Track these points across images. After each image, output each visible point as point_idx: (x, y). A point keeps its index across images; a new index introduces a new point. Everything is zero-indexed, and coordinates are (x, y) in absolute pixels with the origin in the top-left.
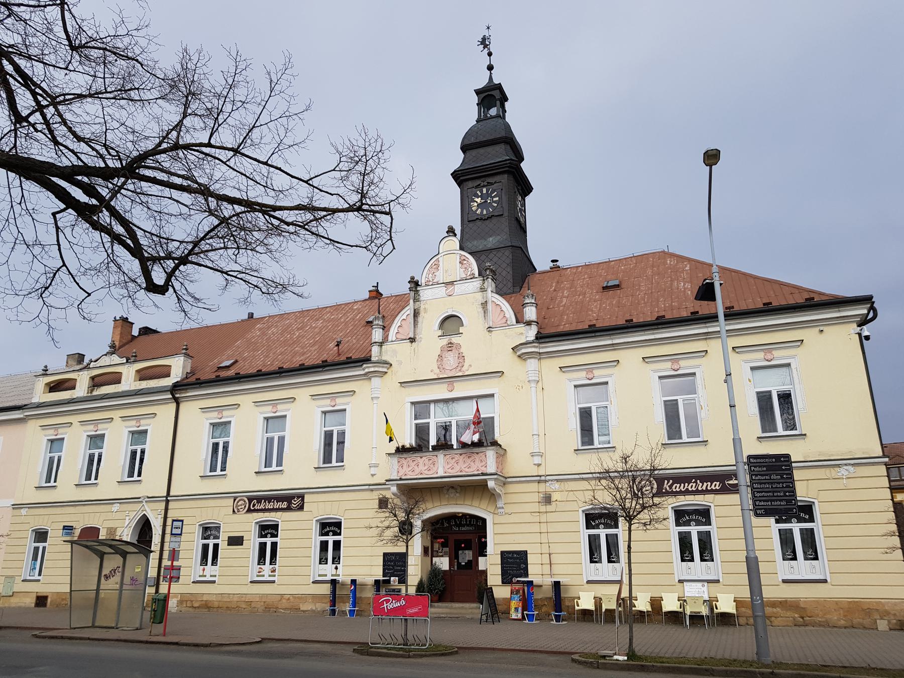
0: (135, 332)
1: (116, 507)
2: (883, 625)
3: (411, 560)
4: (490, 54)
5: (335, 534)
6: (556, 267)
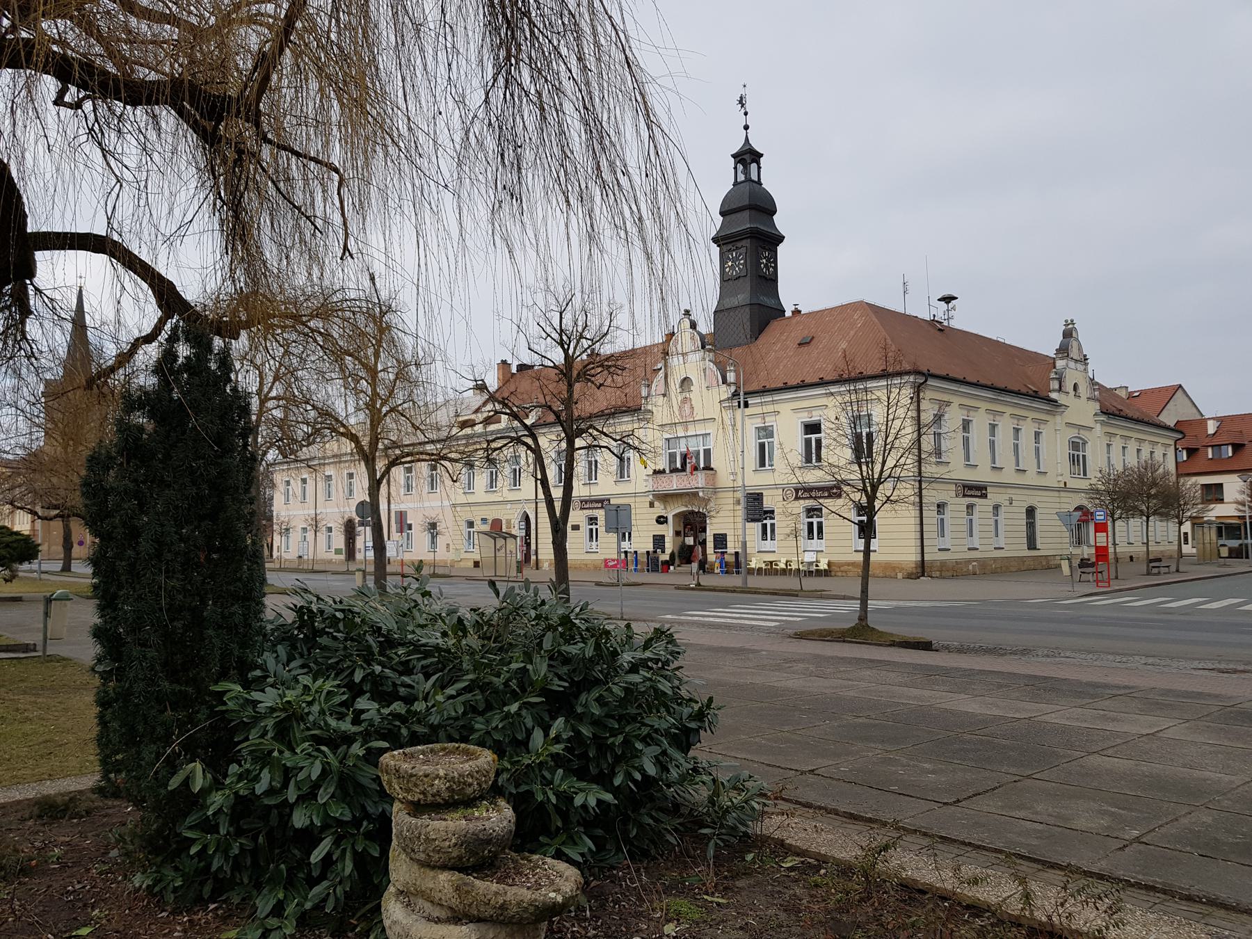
0: (514, 370)
1: (509, 506)
2: (900, 576)
3: (667, 539)
4: (746, 114)
5: (818, 516)
6: (797, 312)
